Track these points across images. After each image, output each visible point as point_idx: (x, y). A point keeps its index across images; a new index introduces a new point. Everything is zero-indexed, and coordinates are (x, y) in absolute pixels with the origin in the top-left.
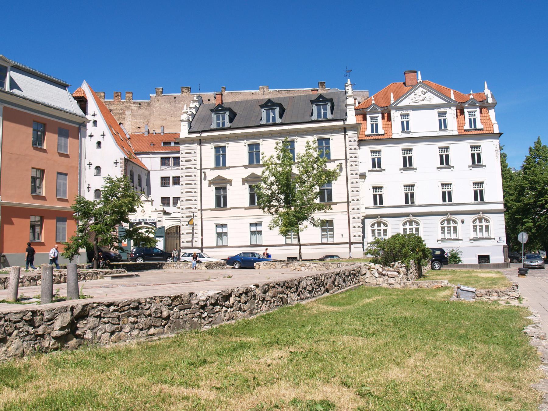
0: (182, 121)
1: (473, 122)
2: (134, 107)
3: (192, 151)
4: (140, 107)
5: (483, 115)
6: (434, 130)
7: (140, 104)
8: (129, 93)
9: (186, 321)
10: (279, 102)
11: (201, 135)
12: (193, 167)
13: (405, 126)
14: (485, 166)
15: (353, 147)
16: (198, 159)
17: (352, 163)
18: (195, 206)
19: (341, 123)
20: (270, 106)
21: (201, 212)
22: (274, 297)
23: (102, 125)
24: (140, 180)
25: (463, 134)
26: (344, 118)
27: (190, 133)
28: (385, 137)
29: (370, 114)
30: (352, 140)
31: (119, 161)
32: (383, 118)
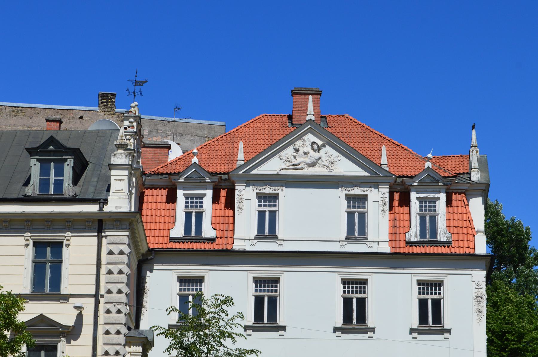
5: (455, 210)
14: (449, 331)
15: (115, 269)
19: (94, 208)
20: (50, 153)
25: (402, 251)
26: (103, 196)
28: (216, 247)
29: (184, 189)
32: (216, 199)
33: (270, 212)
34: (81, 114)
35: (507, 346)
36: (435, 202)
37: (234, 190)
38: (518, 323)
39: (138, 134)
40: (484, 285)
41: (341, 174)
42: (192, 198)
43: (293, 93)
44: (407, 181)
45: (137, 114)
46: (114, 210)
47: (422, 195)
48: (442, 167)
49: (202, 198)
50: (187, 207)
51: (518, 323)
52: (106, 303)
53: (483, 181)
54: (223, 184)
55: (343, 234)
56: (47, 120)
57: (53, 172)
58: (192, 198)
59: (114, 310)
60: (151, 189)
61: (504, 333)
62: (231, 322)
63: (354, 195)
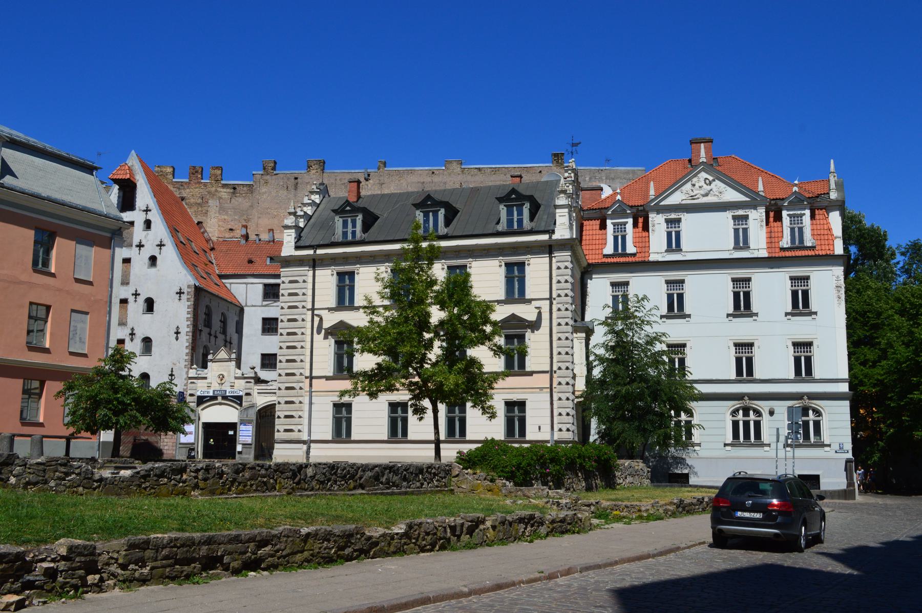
0: (287, 227)
1: (797, 233)
2: (224, 193)
3: (300, 279)
4: (234, 193)
5: (818, 222)
6: (724, 247)
7: (234, 188)
8: (217, 168)
9: (121, 488)
10: (446, 200)
11: (315, 252)
12: (300, 305)
13: (674, 242)
14: (816, 313)
15: (562, 279)
16: (310, 292)
17: (560, 306)
18: (301, 371)
19: (545, 237)
20: (513, 200)
21: (311, 381)
22: (252, 480)
23: (160, 229)
24: (224, 322)
25: (777, 255)
26: (551, 228)
27: (297, 248)
28: (637, 260)
29: (612, 219)
30: (563, 267)
31: (185, 290)
32: (635, 225)
33: (676, 232)
34: (540, 169)
35: (868, 322)
36: (801, 217)
37: (647, 218)
38: (877, 304)
39: (576, 182)
40: (842, 278)
41: (728, 201)
42: (618, 225)
43: (692, 143)
44: (779, 203)
45: (574, 167)
46: (560, 238)
47: (791, 213)
48: (807, 190)
49: (625, 225)
50: (614, 232)
51: (877, 304)
52: (558, 303)
53: (840, 198)
54: (640, 214)
55: (732, 245)
56: (512, 176)
57: (515, 213)
58: (618, 225)
59: (563, 308)
60: (588, 220)
61: (865, 312)
62: (649, 313)
63: (738, 215)
